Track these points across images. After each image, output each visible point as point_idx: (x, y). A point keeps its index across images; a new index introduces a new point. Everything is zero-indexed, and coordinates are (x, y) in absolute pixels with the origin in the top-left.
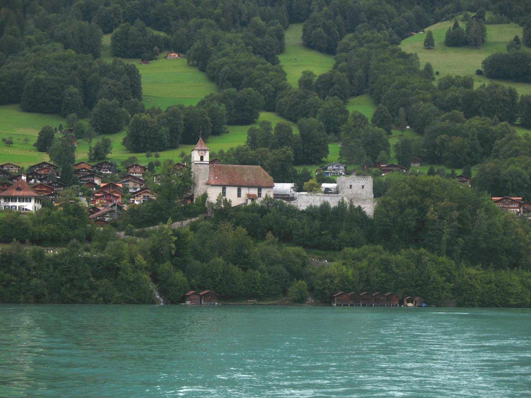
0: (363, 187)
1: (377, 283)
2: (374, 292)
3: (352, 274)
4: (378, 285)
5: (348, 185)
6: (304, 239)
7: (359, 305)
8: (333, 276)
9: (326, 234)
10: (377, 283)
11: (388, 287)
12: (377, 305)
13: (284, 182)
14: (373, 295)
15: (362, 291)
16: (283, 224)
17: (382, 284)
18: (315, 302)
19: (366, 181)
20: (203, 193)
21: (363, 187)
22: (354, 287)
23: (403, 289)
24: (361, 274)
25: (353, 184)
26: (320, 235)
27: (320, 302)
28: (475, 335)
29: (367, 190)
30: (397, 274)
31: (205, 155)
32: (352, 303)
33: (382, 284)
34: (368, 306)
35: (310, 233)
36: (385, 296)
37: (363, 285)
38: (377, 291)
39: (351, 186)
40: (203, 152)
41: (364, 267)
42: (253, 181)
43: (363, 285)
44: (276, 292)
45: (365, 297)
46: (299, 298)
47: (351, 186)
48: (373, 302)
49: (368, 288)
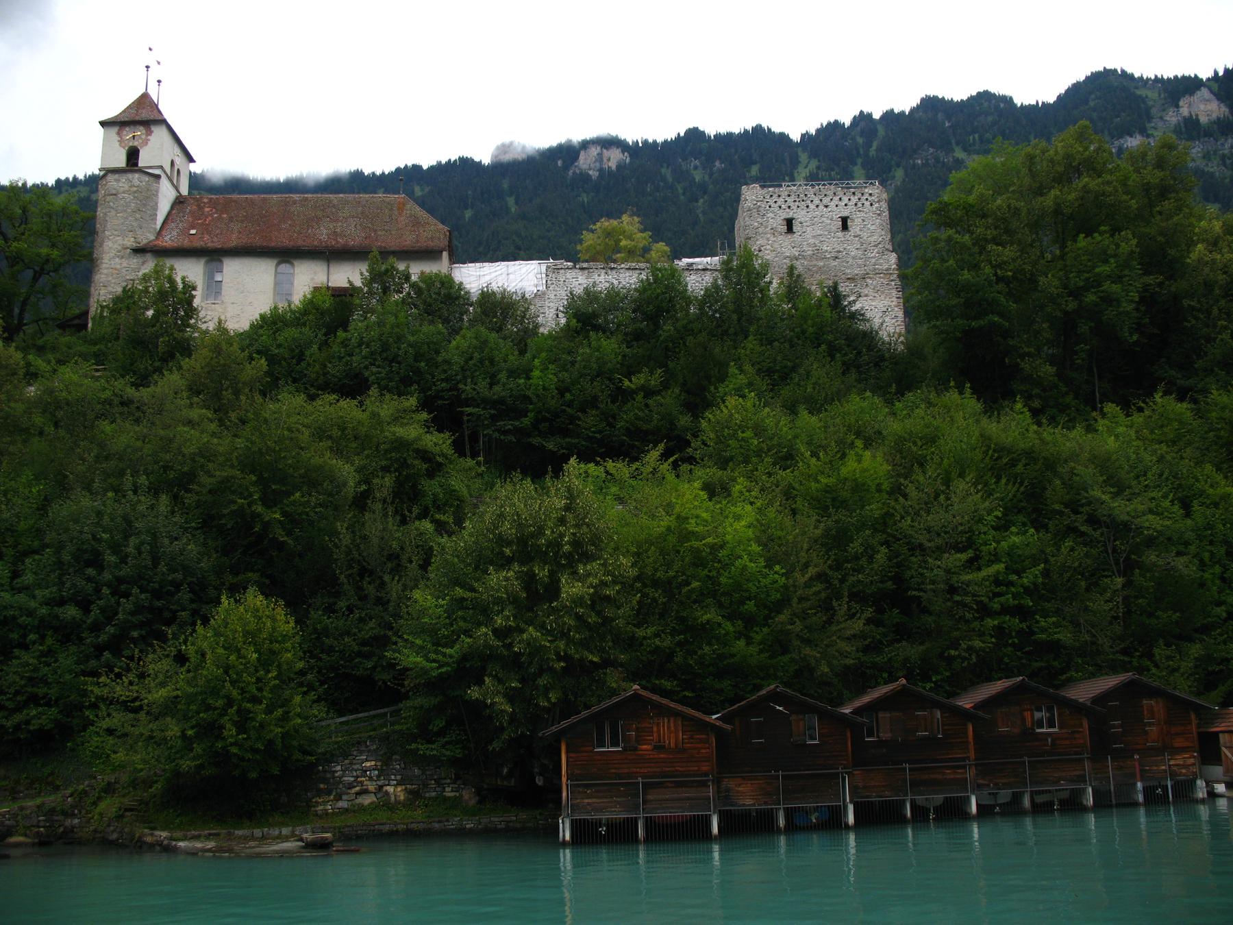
0: (845, 223)
1: (984, 611)
2: (961, 683)
3: (767, 540)
4: (991, 622)
5: (776, 220)
6: (526, 421)
7: (833, 823)
8: (556, 544)
9: (649, 393)
10: (984, 611)
11: (1065, 636)
12: (1005, 795)
13: (514, 258)
14: (966, 702)
15: (858, 679)
16: (418, 357)
17: (1021, 612)
18: (414, 795)
19: (854, 199)
20: (120, 290)
21: (845, 223)
22: (780, 644)
23: (1195, 650)
24: (837, 539)
25: (800, 215)
26: (620, 395)
27: (468, 796)
28: (1173, 815)
29: (865, 235)
30: (1122, 529)
31: (146, 142)
32: (747, 797)
33: (1021, 612)
34: (920, 815)
35: (562, 391)
36: (1076, 708)
37: (858, 625)
38: (983, 671)
39: (789, 223)
40: (140, 132)
41: (858, 488)
42: (353, 235)
43: (858, 625)
44: (41, 718)
45: (885, 729)
46: (186, 764)
47: (789, 223)
48: (970, 774)
49: (912, 651)
